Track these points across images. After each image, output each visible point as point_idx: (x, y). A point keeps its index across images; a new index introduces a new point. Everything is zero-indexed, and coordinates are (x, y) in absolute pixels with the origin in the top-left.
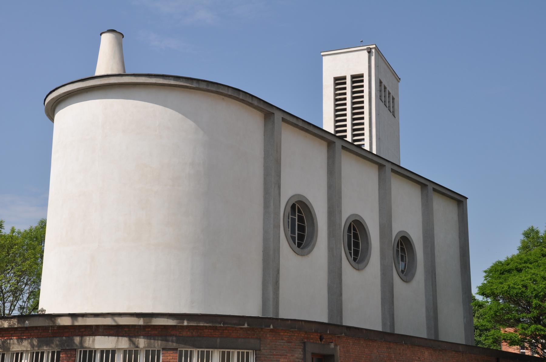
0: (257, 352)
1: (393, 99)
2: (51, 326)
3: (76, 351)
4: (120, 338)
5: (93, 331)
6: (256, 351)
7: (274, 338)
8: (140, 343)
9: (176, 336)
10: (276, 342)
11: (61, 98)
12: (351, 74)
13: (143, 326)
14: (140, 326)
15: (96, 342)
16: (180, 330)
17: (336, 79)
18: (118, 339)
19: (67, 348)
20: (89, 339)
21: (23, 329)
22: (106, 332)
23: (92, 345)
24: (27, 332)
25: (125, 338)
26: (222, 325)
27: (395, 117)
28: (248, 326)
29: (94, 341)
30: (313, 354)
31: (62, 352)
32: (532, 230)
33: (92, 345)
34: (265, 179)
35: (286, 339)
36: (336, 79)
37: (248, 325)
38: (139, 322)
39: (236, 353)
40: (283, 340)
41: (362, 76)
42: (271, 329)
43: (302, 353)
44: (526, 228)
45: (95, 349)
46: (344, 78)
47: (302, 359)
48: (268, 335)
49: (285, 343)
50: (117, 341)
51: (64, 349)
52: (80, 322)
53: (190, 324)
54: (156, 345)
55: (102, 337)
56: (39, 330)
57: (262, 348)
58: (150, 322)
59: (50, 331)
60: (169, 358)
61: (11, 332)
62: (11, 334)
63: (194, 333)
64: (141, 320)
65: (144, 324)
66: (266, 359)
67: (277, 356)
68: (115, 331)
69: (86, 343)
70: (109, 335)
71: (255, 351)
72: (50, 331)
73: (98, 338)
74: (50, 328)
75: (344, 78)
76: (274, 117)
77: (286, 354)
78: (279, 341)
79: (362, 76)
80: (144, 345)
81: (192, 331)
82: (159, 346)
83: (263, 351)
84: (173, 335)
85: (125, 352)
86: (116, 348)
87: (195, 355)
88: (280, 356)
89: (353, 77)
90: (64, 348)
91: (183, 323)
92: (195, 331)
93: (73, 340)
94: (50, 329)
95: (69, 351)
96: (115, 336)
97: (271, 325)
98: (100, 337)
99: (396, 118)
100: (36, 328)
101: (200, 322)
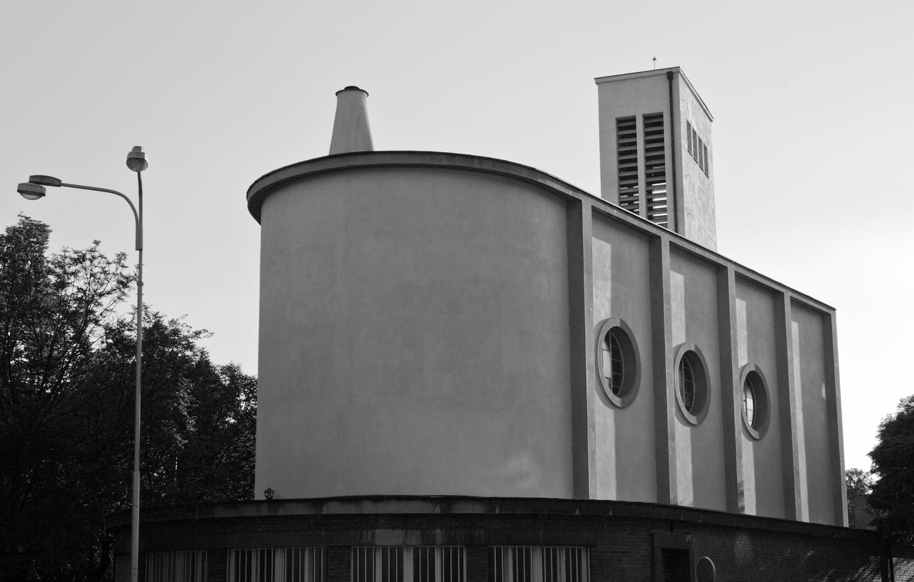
0: (592, 549)
1: (706, 148)
2: (314, 515)
4: (409, 531)
6: (590, 546)
12: (645, 113)
13: (440, 515)
14: (435, 515)
17: (619, 121)
19: (338, 545)
20: (367, 533)
26: (546, 513)
27: (708, 178)
29: (373, 535)
30: (664, 550)
32: (20, 185)
34: (570, 296)
36: (619, 121)
40: (625, 530)
41: (660, 116)
42: (611, 516)
44: (16, 188)
46: (633, 119)
52: (368, 508)
70: (394, 528)
71: (588, 548)
73: (378, 532)
75: (633, 119)
77: (629, 550)
79: (660, 116)
82: (353, 550)
85: (416, 550)
89: (646, 117)
93: (613, 513)
99: (710, 179)
100: (292, 517)
101: (739, 491)
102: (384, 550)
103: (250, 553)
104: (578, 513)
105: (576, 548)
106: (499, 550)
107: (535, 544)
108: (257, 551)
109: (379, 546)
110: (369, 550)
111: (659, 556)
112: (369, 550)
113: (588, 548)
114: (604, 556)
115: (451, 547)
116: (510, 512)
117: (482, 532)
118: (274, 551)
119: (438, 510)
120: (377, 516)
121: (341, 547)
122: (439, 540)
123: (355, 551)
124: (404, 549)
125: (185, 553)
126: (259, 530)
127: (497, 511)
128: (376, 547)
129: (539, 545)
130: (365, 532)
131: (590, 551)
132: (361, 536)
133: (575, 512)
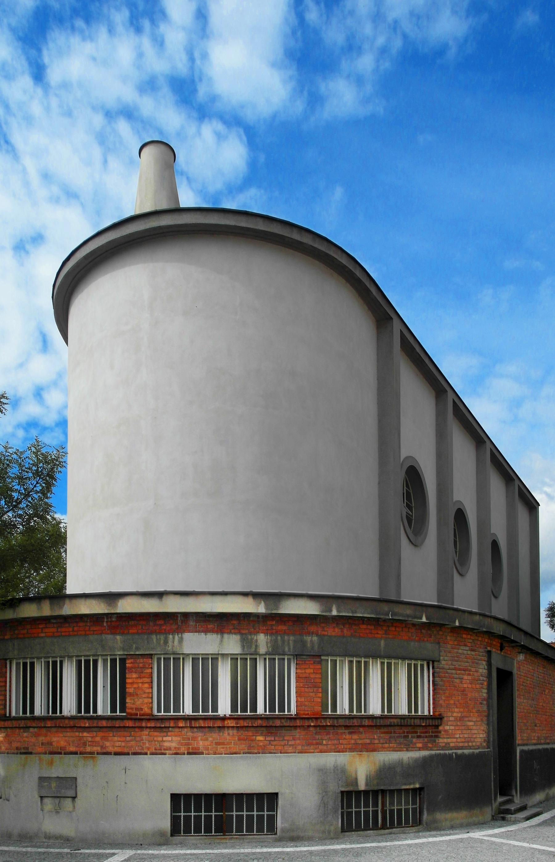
0: (436, 663)
3: (152, 658)
4: (226, 636)
5: (179, 624)
6: (433, 662)
7: (456, 643)
8: (259, 645)
9: (317, 635)
10: (458, 649)
11: (81, 270)
15: (185, 643)
16: (323, 625)
18: (222, 637)
20: (174, 638)
21: (59, 621)
22: (200, 626)
23: (178, 648)
24: (67, 625)
25: (234, 636)
28: (427, 620)
29: (181, 640)
31: (128, 660)
33: (178, 648)
35: (469, 644)
37: (427, 619)
38: (258, 609)
39: (379, 665)
40: (465, 645)
43: (486, 667)
45: (177, 839)
47: (487, 677)
48: (449, 638)
49: (468, 650)
50: (221, 641)
51: (132, 654)
53: (341, 614)
54: (286, 649)
55: (195, 633)
56: (87, 622)
57: (441, 658)
58: (277, 608)
59: (105, 624)
60: (308, 671)
61: (41, 626)
62: (40, 630)
63: (345, 631)
64: (260, 606)
65: (266, 611)
66: (447, 675)
67: (459, 672)
68: (216, 624)
69: (168, 645)
71: (431, 663)
72: (105, 624)
73: (187, 636)
74: (104, 618)
76: (393, 325)
78: (462, 648)
80: (266, 648)
81: (342, 627)
83: (443, 662)
84: (313, 633)
85: (234, 660)
86: (220, 653)
87: (260, 670)
88: (464, 671)
90: (133, 653)
91: (331, 611)
92: (347, 626)
94: (105, 620)
95: (140, 657)
96: (217, 632)
97: (456, 620)
98: (192, 634)
102: (195, 660)
103: (32, 665)
104: (424, 620)
105: (355, 660)
106: (334, 663)
107: (375, 656)
108: (265, 659)
109: (188, 655)
110: (176, 660)
111: (494, 674)
112: (176, 660)
113: (431, 663)
114: (447, 673)
115: (277, 657)
116: (350, 615)
117: (315, 638)
118: (183, 659)
119: (261, 609)
120: (186, 615)
121: (142, 655)
122: (263, 650)
123: (159, 660)
124: (220, 659)
125: (265, 659)
126: (43, 635)
127: (334, 613)
128: (184, 656)
129: (381, 657)
130: (171, 636)
131: (433, 668)
132: (166, 642)
133: (421, 618)
